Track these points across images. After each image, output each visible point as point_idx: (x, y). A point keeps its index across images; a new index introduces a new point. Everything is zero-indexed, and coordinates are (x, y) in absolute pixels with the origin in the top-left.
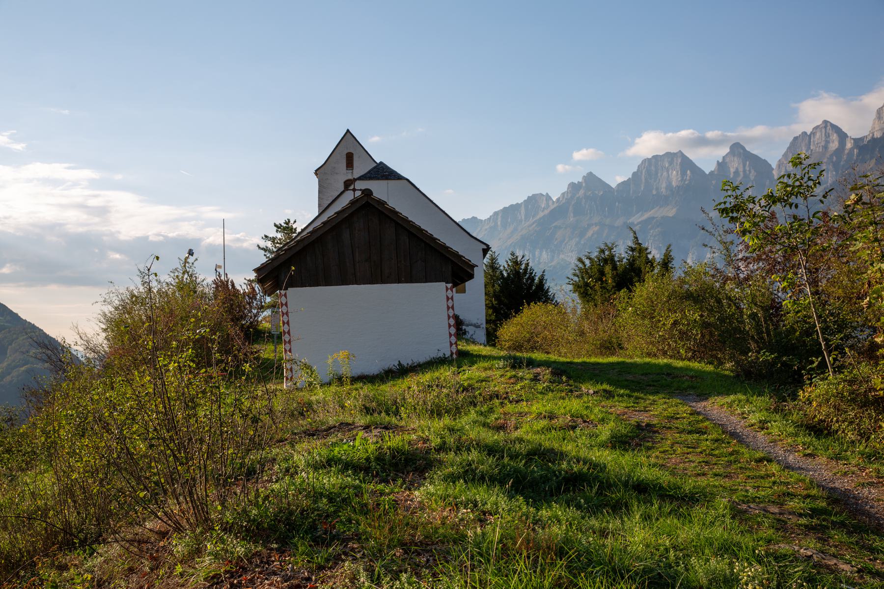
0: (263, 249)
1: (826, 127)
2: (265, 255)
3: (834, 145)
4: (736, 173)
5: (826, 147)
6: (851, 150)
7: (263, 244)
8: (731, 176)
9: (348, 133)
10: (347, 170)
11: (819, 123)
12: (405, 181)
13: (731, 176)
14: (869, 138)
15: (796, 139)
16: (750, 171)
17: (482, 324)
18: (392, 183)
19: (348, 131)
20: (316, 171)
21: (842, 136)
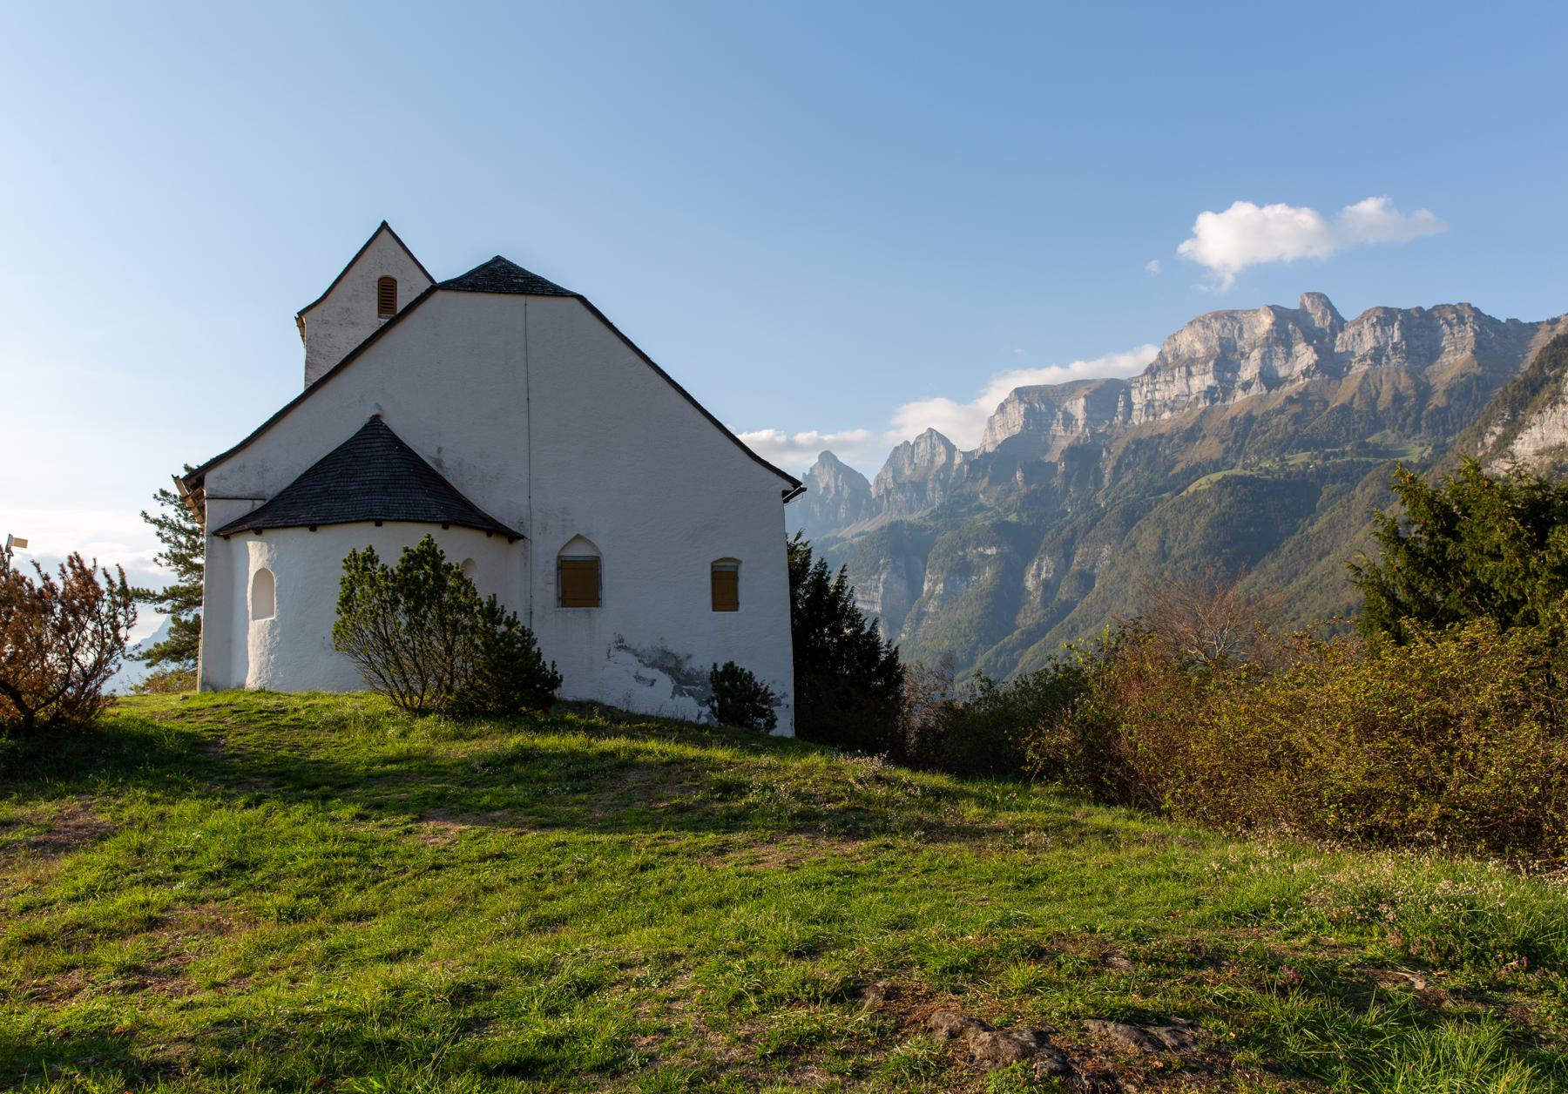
0: (155, 521)
1: (931, 436)
2: (159, 534)
3: (941, 459)
4: (827, 488)
5: (931, 461)
6: (961, 465)
7: (157, 511)
8: (821, 493)
9: (385, 233)
10: (380, 317)
11: (924, 430)
12: (575, 302)
13: (821, 493)
14: (980, 452)
15: (897, 449)
16: (843, 489)
17: (785, 695)
18: (537, 303)
19: (384, 225)
20: (301, 313)
21: (951, 449)
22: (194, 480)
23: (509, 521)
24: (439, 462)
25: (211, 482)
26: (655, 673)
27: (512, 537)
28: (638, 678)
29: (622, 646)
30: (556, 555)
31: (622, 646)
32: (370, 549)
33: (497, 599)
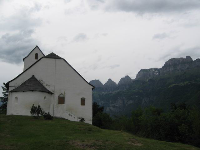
9: (37, 47)
18: (42, 90)
19: (37, 46)
22: (7, 85)
25: (10, 85)
32: (103, 107)
33: (81, 117)
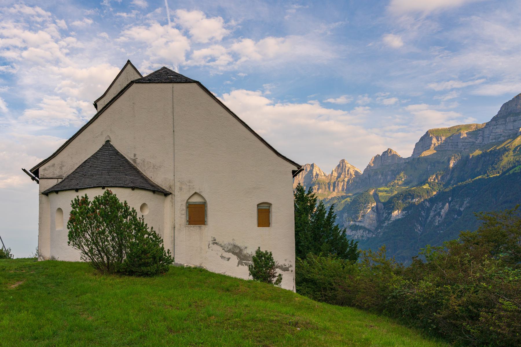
9: (129, 65)
23: (165, 186)
24: (135, 161)
26: (230, 255)
27: (166, 194)
28: (222, 257)
29: (215, 242)
30: (184, 203)
31: (215, 242)
